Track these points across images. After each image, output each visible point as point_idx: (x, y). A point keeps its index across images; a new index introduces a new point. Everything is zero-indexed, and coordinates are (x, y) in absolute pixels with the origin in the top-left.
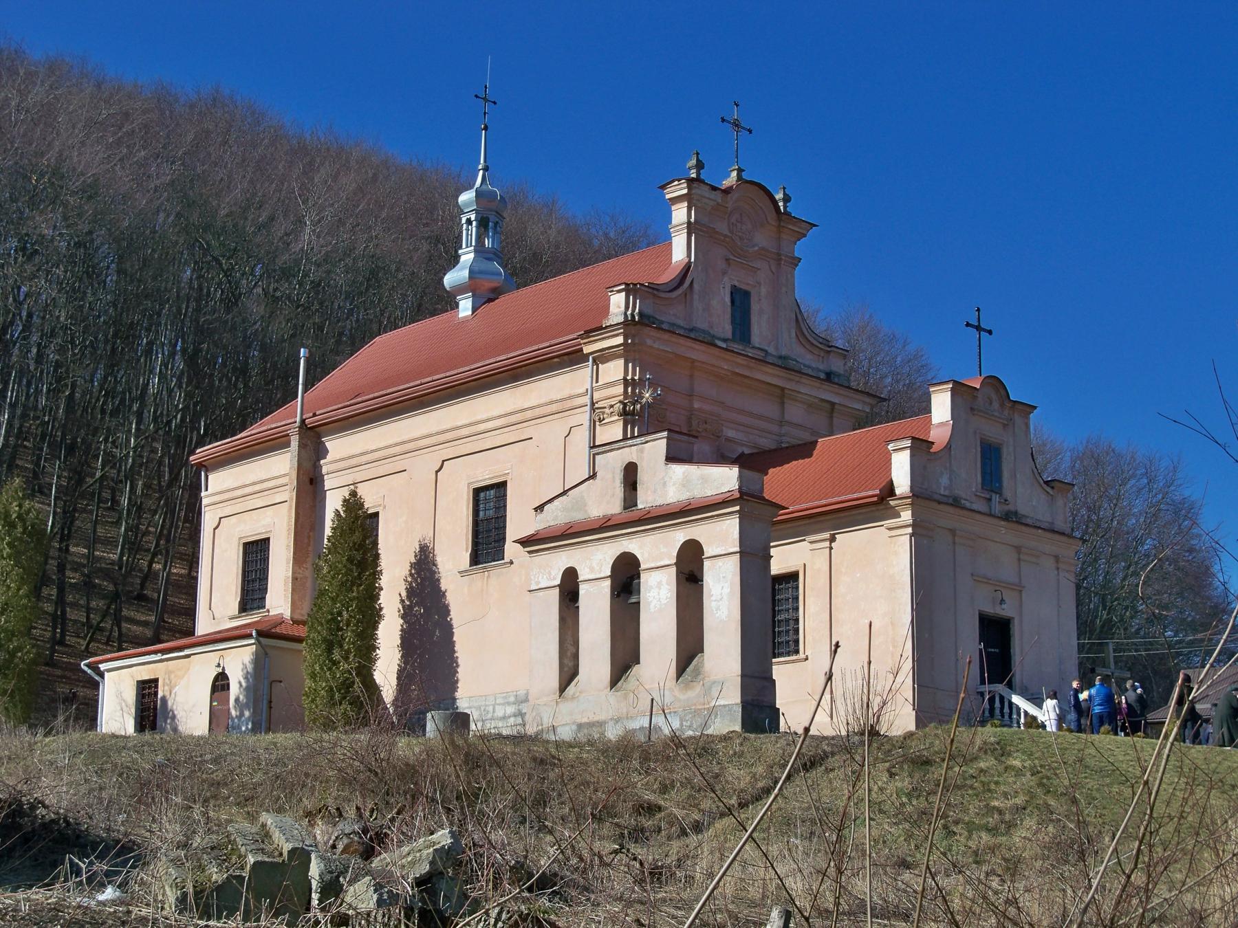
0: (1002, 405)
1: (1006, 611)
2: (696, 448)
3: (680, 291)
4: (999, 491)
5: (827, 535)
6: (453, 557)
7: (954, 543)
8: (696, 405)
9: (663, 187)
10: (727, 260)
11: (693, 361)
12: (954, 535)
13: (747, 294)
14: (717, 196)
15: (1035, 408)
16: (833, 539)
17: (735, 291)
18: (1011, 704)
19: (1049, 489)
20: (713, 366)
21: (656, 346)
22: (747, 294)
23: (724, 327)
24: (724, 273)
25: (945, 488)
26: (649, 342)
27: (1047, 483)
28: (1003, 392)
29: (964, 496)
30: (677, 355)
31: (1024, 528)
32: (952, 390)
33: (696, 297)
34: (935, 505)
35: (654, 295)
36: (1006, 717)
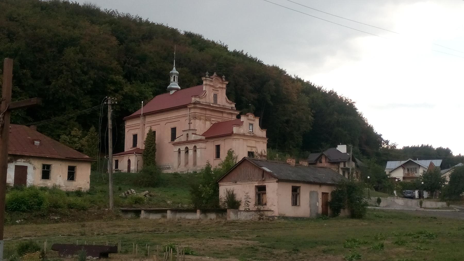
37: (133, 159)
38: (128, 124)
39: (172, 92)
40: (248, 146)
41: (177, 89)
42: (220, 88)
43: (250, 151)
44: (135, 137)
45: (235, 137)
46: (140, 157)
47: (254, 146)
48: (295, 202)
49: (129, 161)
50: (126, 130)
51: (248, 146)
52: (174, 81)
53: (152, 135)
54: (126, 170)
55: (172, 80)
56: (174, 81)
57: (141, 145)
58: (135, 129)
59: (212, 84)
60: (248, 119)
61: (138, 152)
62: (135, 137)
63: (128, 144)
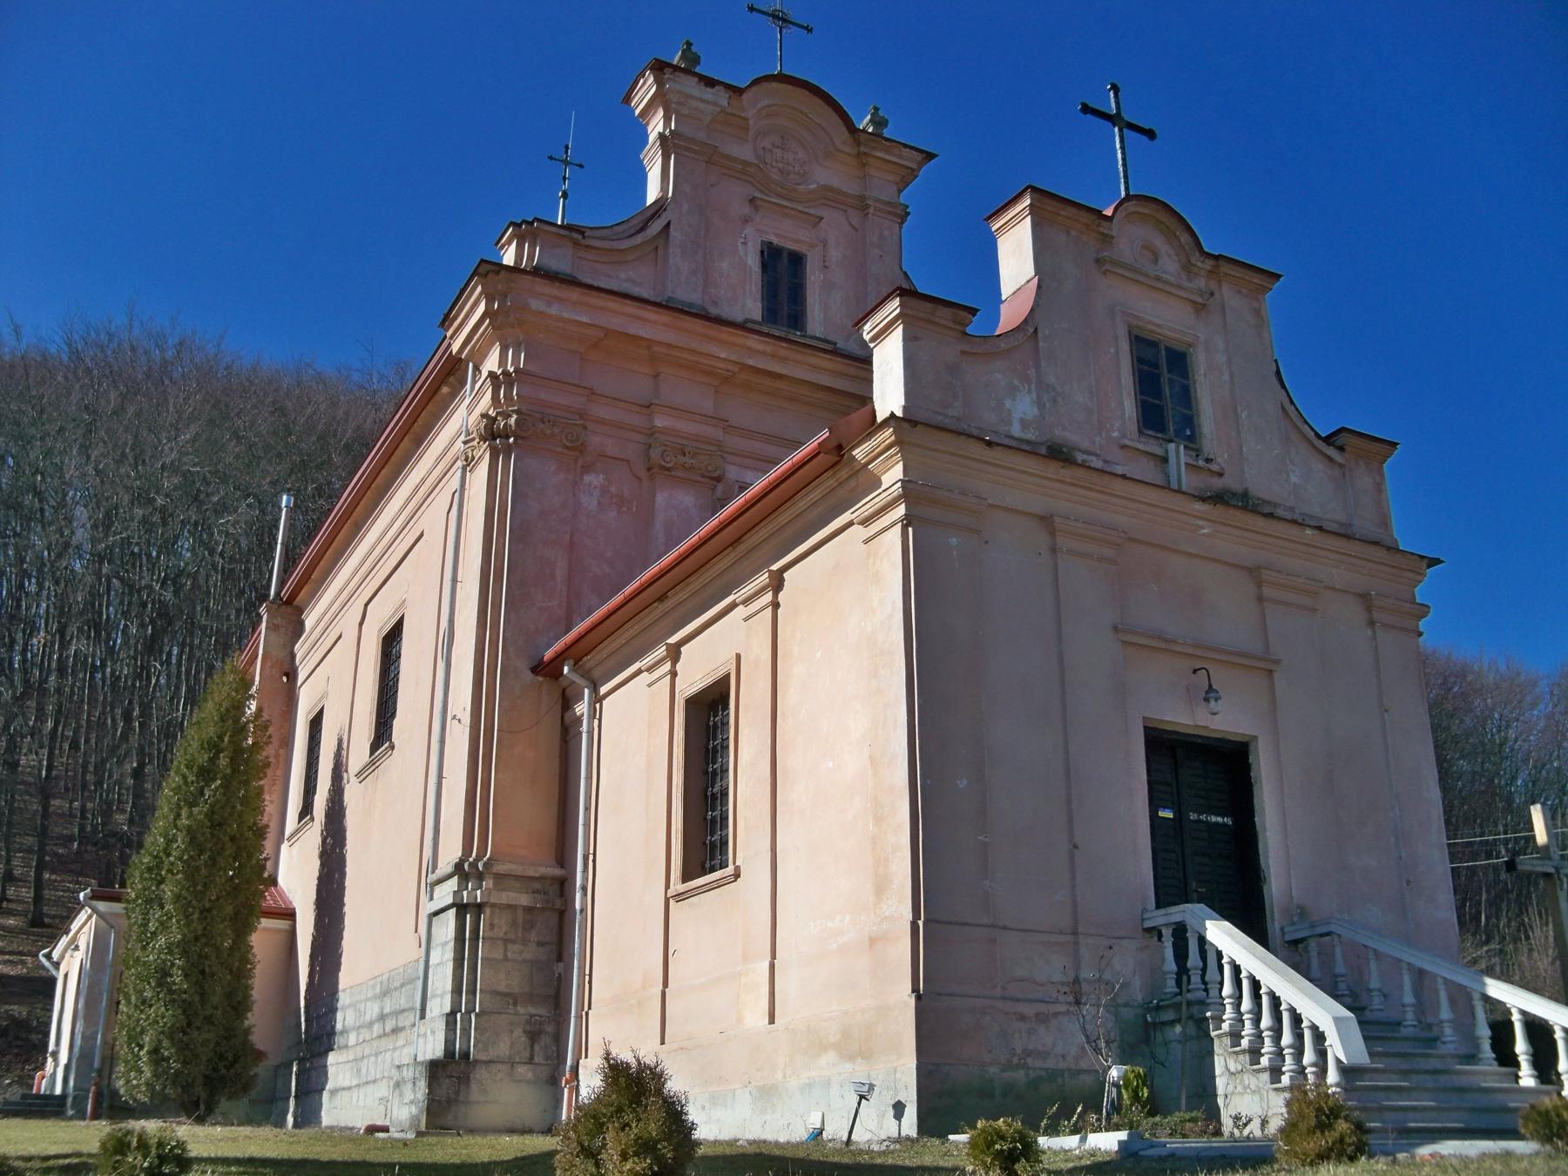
0: (1188, 267)
1: (1224, 719)
2: (661, 498)
3: (639, 239)
4: (1188, 430)
5: (763, 578)
6: (358, 755)
7: (1054, 550)
8: (659, 422)
9: (627, 99)
10: (752, 201)
11: (650, 343)
12: (1052, 533)
13: (797, 260)
14: (722, 97)
15: (1277, 277)
16: (777, 583)
17: (771, 256)
18: (1202, 940)
19: (1331, 451)
20: (693, 352)
21: (553, 310)
22: (797, 260)
23: (752, 307)
24: (746, 220)
25: (1024, 424)
26: (535, 304)
27: (1328, 440)
28: (1185, 238)
29: (1085, 445)
30: (608, 332)
31: (1261, 523)
32: (1033, 210)
33: (674, 250)
34: (977, 449)
35: (576, 243)
36: (1195, 979)
42: (830, 197)
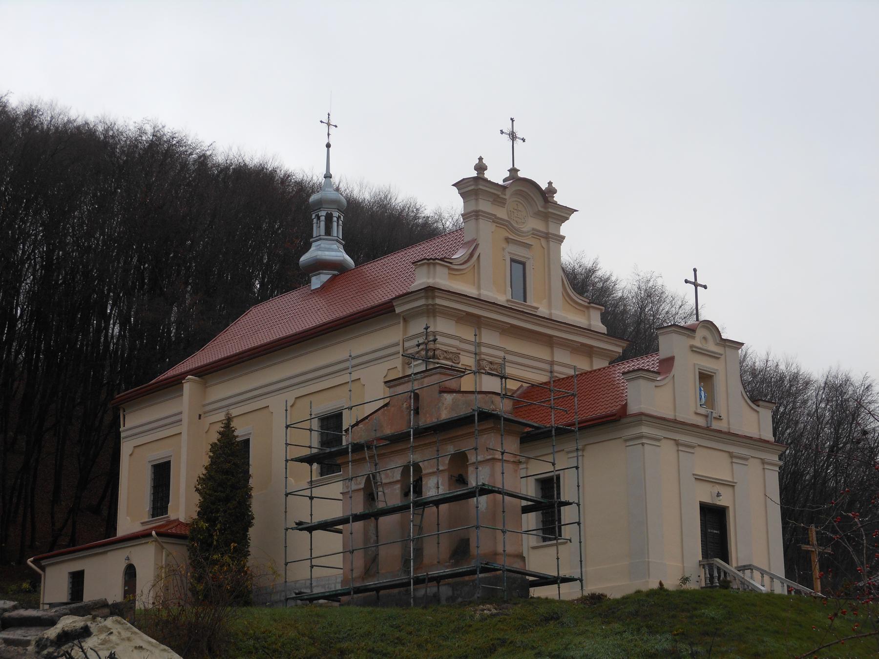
35: (449, 268)
37: (147, 560)
38: (134, 421)
39: (317, 282)
40: (699, 479)
41: (337, 267)
42: (536, 233)
43: (707, 499)
44: (162, 474)
45: (645, 430)
46: (179, 554)
47: (727, 477)
48: (77, 579)
49: (130, 572)
50: (126, 448)
51: (699, 479)
52: (328, 232)
53: (229, 463)
54: (341, 571)
55: (319, 229)
56: (328, 232)
57: (184, 505)
58: (163, 440)
59: (501, 213)
60: (694, 350)
61: (168, 534)
62: (162, 474)
63: (132, 511)
